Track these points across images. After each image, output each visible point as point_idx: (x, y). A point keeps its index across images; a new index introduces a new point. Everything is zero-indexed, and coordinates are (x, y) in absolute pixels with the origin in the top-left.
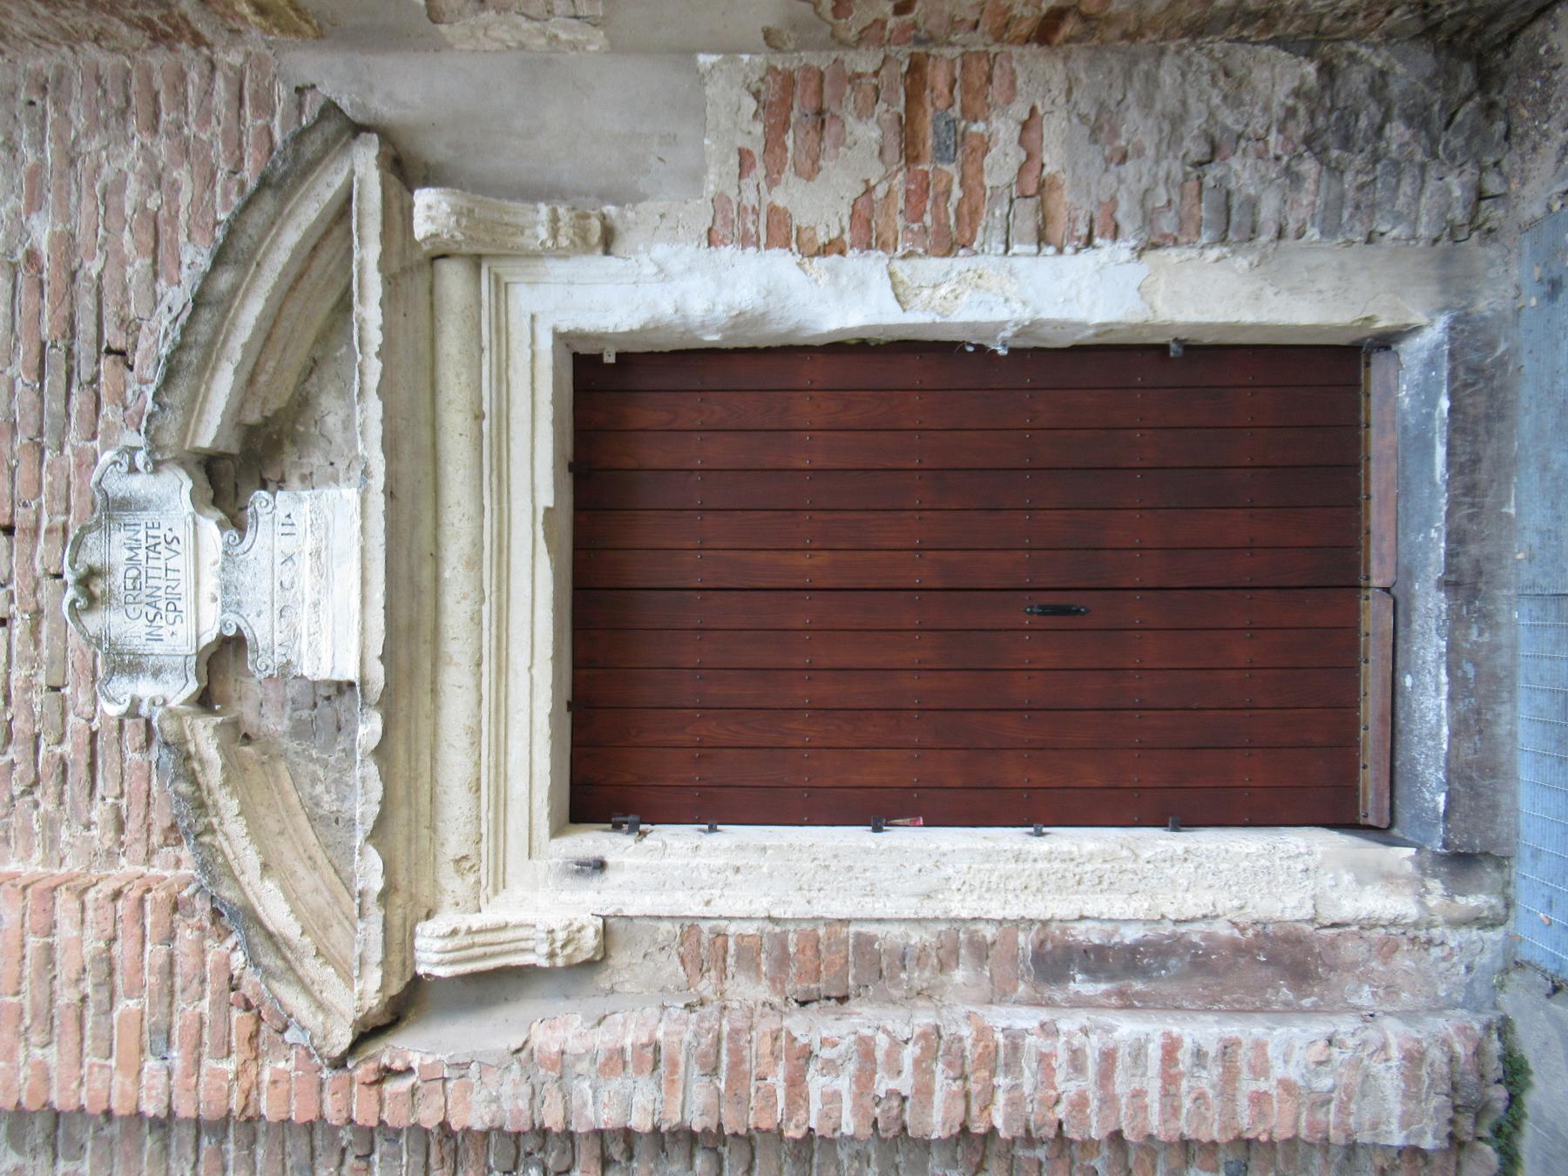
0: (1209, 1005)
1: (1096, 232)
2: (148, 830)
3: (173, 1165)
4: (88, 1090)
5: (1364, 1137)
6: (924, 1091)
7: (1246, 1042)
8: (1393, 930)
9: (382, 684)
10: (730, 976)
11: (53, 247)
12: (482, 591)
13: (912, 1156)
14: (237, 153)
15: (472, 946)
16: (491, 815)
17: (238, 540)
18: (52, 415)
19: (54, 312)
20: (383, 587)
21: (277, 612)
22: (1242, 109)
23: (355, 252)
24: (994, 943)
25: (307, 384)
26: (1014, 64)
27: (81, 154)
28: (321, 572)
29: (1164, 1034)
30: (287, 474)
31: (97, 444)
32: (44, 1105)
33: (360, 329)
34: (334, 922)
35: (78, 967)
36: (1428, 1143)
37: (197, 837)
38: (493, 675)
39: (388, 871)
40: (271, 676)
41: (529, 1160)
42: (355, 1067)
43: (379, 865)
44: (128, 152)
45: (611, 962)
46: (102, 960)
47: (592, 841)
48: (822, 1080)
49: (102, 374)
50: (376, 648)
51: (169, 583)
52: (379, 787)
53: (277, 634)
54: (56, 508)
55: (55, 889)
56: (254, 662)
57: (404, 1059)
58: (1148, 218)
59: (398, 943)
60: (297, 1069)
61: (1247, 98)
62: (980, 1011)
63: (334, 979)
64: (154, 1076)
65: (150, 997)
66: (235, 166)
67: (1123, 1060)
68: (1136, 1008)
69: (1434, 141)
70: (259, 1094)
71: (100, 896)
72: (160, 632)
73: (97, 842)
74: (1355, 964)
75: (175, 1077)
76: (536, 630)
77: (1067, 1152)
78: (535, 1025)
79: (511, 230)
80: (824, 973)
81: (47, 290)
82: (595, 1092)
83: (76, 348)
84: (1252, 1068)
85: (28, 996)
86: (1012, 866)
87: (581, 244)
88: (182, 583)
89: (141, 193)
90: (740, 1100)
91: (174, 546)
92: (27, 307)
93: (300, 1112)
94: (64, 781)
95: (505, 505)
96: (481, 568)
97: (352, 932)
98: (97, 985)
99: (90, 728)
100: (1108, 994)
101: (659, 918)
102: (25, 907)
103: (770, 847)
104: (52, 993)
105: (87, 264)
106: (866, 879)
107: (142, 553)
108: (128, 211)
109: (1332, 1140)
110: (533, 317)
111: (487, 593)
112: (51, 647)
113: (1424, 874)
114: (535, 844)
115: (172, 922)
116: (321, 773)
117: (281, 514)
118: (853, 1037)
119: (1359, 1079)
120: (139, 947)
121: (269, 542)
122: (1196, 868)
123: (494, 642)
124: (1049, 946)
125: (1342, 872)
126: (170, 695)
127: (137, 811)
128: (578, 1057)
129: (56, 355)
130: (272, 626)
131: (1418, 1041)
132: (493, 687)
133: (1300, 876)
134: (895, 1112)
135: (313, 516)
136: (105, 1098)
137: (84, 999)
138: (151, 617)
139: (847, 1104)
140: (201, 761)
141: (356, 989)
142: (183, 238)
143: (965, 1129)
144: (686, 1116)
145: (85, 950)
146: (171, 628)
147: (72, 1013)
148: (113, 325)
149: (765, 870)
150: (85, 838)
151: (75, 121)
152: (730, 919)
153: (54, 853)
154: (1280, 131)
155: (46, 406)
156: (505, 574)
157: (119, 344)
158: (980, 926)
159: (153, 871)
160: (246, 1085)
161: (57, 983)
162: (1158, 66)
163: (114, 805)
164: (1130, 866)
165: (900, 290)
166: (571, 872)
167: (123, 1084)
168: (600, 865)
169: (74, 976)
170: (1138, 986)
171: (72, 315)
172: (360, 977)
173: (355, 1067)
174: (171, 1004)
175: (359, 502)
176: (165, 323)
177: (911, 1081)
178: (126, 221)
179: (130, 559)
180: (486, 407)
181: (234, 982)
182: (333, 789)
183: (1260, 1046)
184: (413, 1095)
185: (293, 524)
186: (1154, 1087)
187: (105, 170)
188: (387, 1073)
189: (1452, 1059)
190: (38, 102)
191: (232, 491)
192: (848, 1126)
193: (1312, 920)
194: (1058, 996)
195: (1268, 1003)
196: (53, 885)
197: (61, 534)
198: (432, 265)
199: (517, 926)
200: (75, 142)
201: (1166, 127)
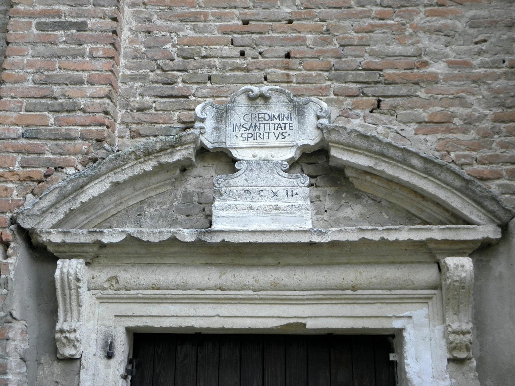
2: (138, 123)
4: (10, 101)
9: (210, 241)
11: (430, 74)
14: (487, 162)
16: (140, 295)
17: (283, 169)
18: (346, 75)
19: (397, 75)
21: (247, 188)
25: (367, 198)
27: (479, 86)
28: (267, 210)
30: (320, 188)
31: (332, 96)
32: (3, 81)
34: (87, 216)
35: (71, 96)
38: (214, 296)
39: (111, 245)
40: (215, 186)
44: (482, 108)
45: (56, 363)
46: (75, 107)
51: (262, 134)
52: (157, 240)
53: (236, 189)
55: (110, 85)
56: (222, 178)
57: (13, 255)
60: (12, 200)
63: (58, 219)
64: (14, 132)
65: (54, 129)
66: (480, 161)
71: (106, 105)
72: (237, 130)
73: (133, 99)
75: (13, 141)
76: (239, 319)
78: (24, 322)
79: (456, 308)
83: (380, 85)
85: (58, 73)
87: (452, 347)
88: (262, 141)
89: (461, 115)
91: (281, 137)
92: (400, 62)
94: (164, 84)
95: (307, 302)
96: (273, 290)
97: (79, 226)
98: (62, 104)
99: (190, 95)
102: (102, 71)
104: (59, 84)
105: (423, 90)
108: (452, 109)
110: (410, 317)
111: (259, 293)
112: (230, 77)
114: (123, 319)
115: (91, 139)
116: (165, 207)
117: (297, 190)
120: (80, 124)
121: (283, 184)
123: (232, 296)
126: (205, 135)
127: (148, 118)
129: (376, 76)
132: (208, 296)
135: (297, 206)
136: (5, 109)
137: (56, 98)
138: (245, 126)
141: (52, 230)
142: (439, 136)
146: (239, 135)
147: (48, 93)
148: (393, 102)
151: (496, 83)
153: (129, 80)
155: (350, 72)
156: (269, 302)
157: (382, 104)
159: (118, 126)
160: (6, 176)
161: (64, 86)
163: (152, 107)
167: (11, 117)
168: (110, 356)
169: (67, 94)
171: (397, 83)
172: (59, 232)
173: (11, 230)
174: (51, 139)
175: (305, 229)
176: (395, 128)
178: (446, 108)
179: (274, 116)
180: (359, 292)
181: (60, 169)
182: (157, 213)
185: (292, 196)
191: (311, 161)
196: (113, 84)
197: (287, 81)
198: (435, 262)
200: (485, 83)
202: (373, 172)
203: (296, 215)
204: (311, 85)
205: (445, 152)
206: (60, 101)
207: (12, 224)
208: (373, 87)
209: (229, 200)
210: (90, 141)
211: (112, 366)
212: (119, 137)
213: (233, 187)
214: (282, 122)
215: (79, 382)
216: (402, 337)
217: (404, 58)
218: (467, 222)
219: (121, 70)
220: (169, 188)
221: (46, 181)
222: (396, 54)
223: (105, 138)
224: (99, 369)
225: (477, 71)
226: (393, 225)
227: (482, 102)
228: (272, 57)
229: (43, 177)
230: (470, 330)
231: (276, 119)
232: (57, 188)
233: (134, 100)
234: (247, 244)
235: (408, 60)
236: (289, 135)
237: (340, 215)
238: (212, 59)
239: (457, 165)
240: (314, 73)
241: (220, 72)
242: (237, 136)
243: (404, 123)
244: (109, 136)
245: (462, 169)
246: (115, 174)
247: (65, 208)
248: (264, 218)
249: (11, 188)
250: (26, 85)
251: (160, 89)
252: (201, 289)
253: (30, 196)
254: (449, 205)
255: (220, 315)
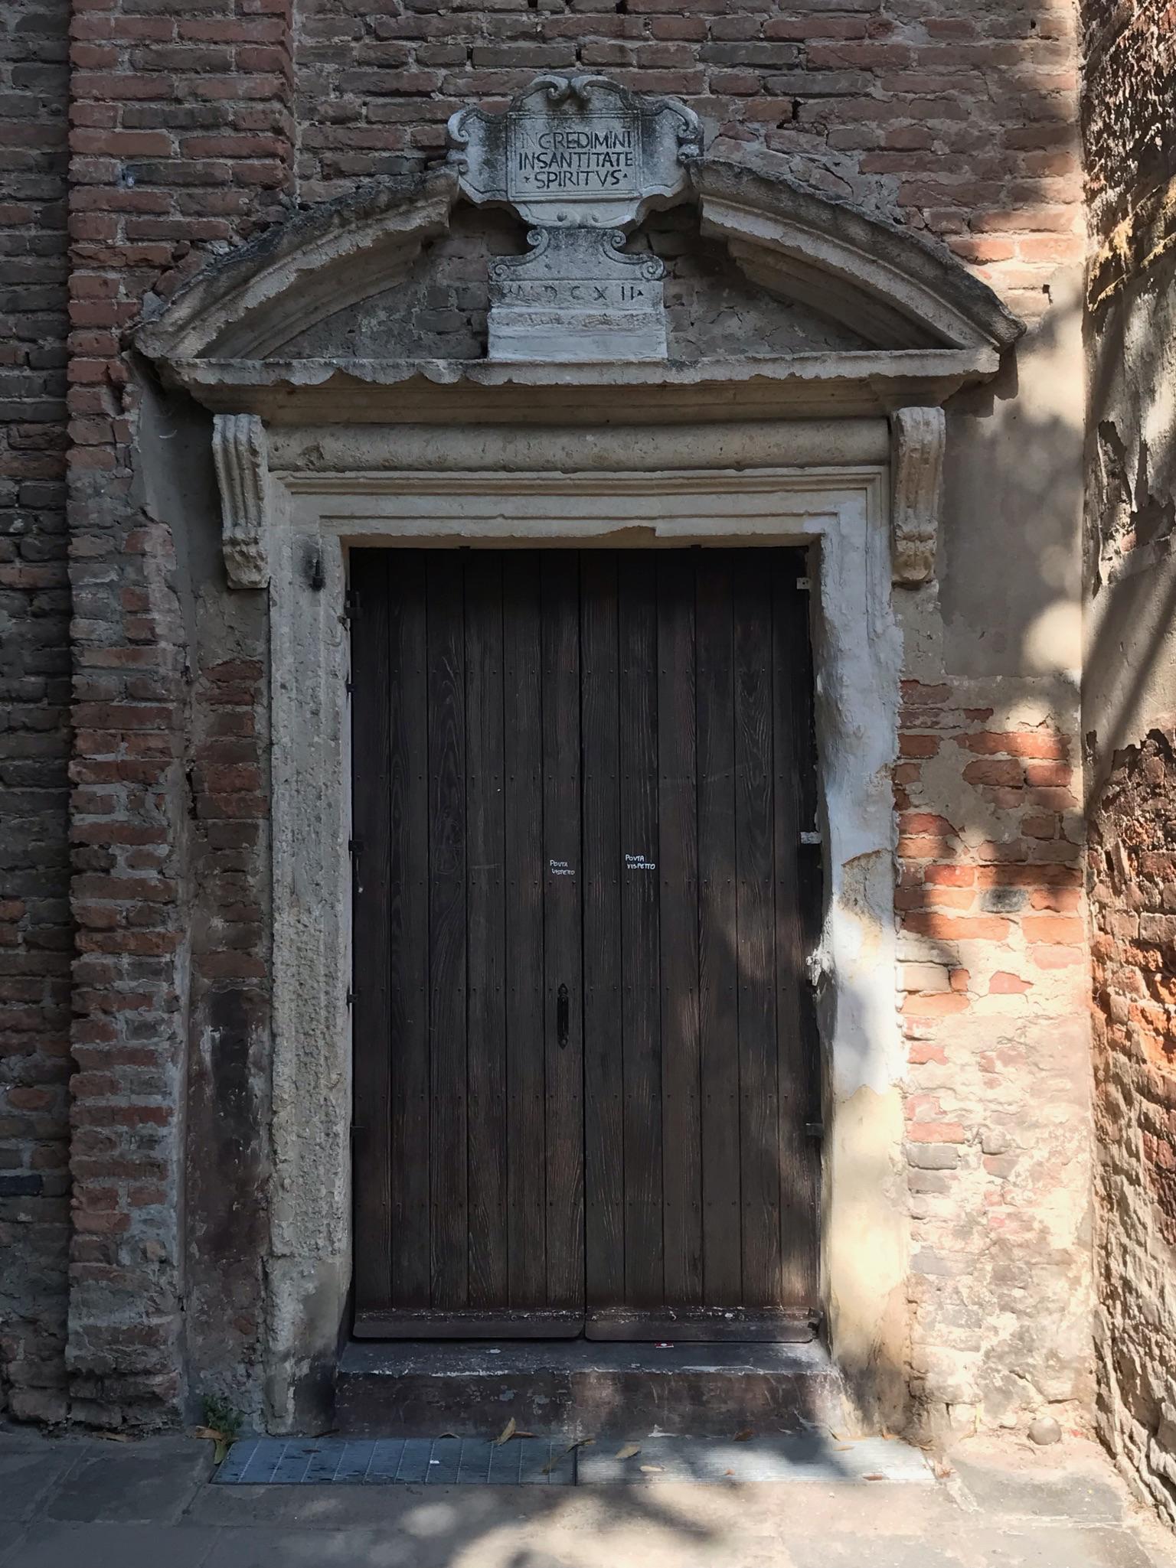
0: (191, 1156)
1: (916, 1043)
2: (336, 149)
3: (13, 176)
5: (75, 1294)
6: (115, 890)
7: (164, 1185)
8: (261, 1330)
9: (485, 383)
10: (214, 707)
11: (894, 47)
12: (575, 470)
13: (43, 881)
15: (241, 469)
17: (615, 245)
20: (575, 383)
22: (1030, 1180)
23: (888, 352)
24: (249, 954)
26: (1071, 966)
28: (587, 325)
29: (171, 1109)
30: (682, 280)
31: (707, 95)
32: (75, 63)
33: (816, 359)
36: (71, 1352)
37: (337, 211)
39: (307, 389)
40: (490, 278)
41: (31, 519)
42: (122, 359)
43: (315, 381)
44: (987, 120)
45: (225, 595)
47: (336, 573)
48: (124, 795)
49: (775, 98)
50: (521, 378)
51: (575, 174)
52: (390, 381)
53: (529, 283)
54: (644, 56)
55: (282, 72)
56: (503, 262)
58: (928, 1092)
59: (235, 401)
60: (118, 304)
61: (1040, 1184)
62: (187, 942)
67: (147, 1071)
68: (189, 1089)
69: (1000, 1357)
70: (93, 268)
72: (528, 166)
73: (323, 99)
74: (228, 1293)
75: (107, 188)
77: (49, 1027)
80: (219, 796)
81: (853, 43)
82: (107, 584)
84: (141, 1190)
86: (322, 971)
88: (576, 188)
90: (102, 720)
91: (610, 179)
93: (78, 307)
97: (242, 354)
98: (191, 113)
99: (433, 91)
100: (201, 1062)
101: (269, 641)
102: (263, 43)
103: (338, 744)
104: (183, 71)
105: (878, 83)
106: (309, 833)
107: (603, 149)
108: (930, 123)
109: (73, 1265)
110: (835, 514)
111: (572, 476)
112: (510, 51)
113: (315, 1359)
114: (335, 522)
115: (254, 184)
116: (397, 316)
117: (641, 286)
118: (165, 823)
119: (129, 1289)
120: (229, 153)
121: (615, 275)
122: (319, 1145)
124: (246, 1006)
125: (316, 1283)
126: (468, 177)
127: (355, 139)
128: (140, 570)
130: (537, 279)
131: (165, 1342)
133: (313, 1242)
134: (94, 863)
135: (641, 317)
138: (542, 158)
139: (103, 819)
140: (408, 212)
141: (198, 361)
142: (904, 176)
143: (78, 927)
144: (86, 670)
145: (225, 102)
146: (532, 177)
147: (163, 89)
149: (316, 739)
150: (327, 87)
152: (269, 707)
153: (312, 58)
154: (1009, 1215)
157: (802, 114)
158: (266, 942)
159: (297, 154)
160: (102, 257)
161: (193, 75)
162: (1070, 1101)
163: (360, 114)
164: (322, 1081)
165: (863, 862)
166: (310, 557)
168: (317, 584)
169: (200, 91)
170: (209, 1091)
171: (830, 69)
172: (210, 364)
173: (122, 359)
176: (824, 159)
177: (124, 877)
178: (921, 120)
180: (748, 472)
182: (382, 328)
183: (161, 1197)
184: (98, 415)
185: (632, 297)
186: (120, 1101)
187: (970, 99)
188: (117, 390)
189: (148, 1373)
190: (1033, 32)
192: (83, 821)
193: (271, 1254)
194: (199, 1015)
195: (193, 1213)
199: (260, 511)
200: (995, 69)
201: (1013, 1109)
202: (779, 249)
203: (640, 333)
204: (667, 71)
205: (914, 209)
206: (187, 106)
207: (123, 349)
208: (785, 75)
209: (517, 305)
210: (252, 187)
211: (323, 602)
212: (300, 178)
213: (524, 280)
214: (613, 150)
215: (270, 627)
216: (819, 550)
217: (845, 14)
218: (944, 343)
219: (296, 38)
220: (402, 280)
221: (177, 267)
222: (830, 7)
223: (280, 183)
224: (301, 607)
225: (982, 43)
226: (814, 350)
227: (986, 110)
228: (591, 11)
229: (170, 259)
230: (933, 533)
231: (601, 144)
232: (202, 281)
233: (326, 101)
234: (551, 386)
235: (853, 20)
236: (625, 176)
237: (717, 330)
238: (473, 14)
239: (933, 233)
240: (672, 46)
241: (491, 41)
242: (527, 179)
243: (841, 150)
244: (286, 178)
245: (943, 241)
246: (304, 253)
247: (218, 319)
248: (582, 339)
249: (113, 280)
250: (119, 72)
251: (374, 79)
252: (470, 469)
253: (150, 294)
254: (912, 312)
255: (506, 515)
